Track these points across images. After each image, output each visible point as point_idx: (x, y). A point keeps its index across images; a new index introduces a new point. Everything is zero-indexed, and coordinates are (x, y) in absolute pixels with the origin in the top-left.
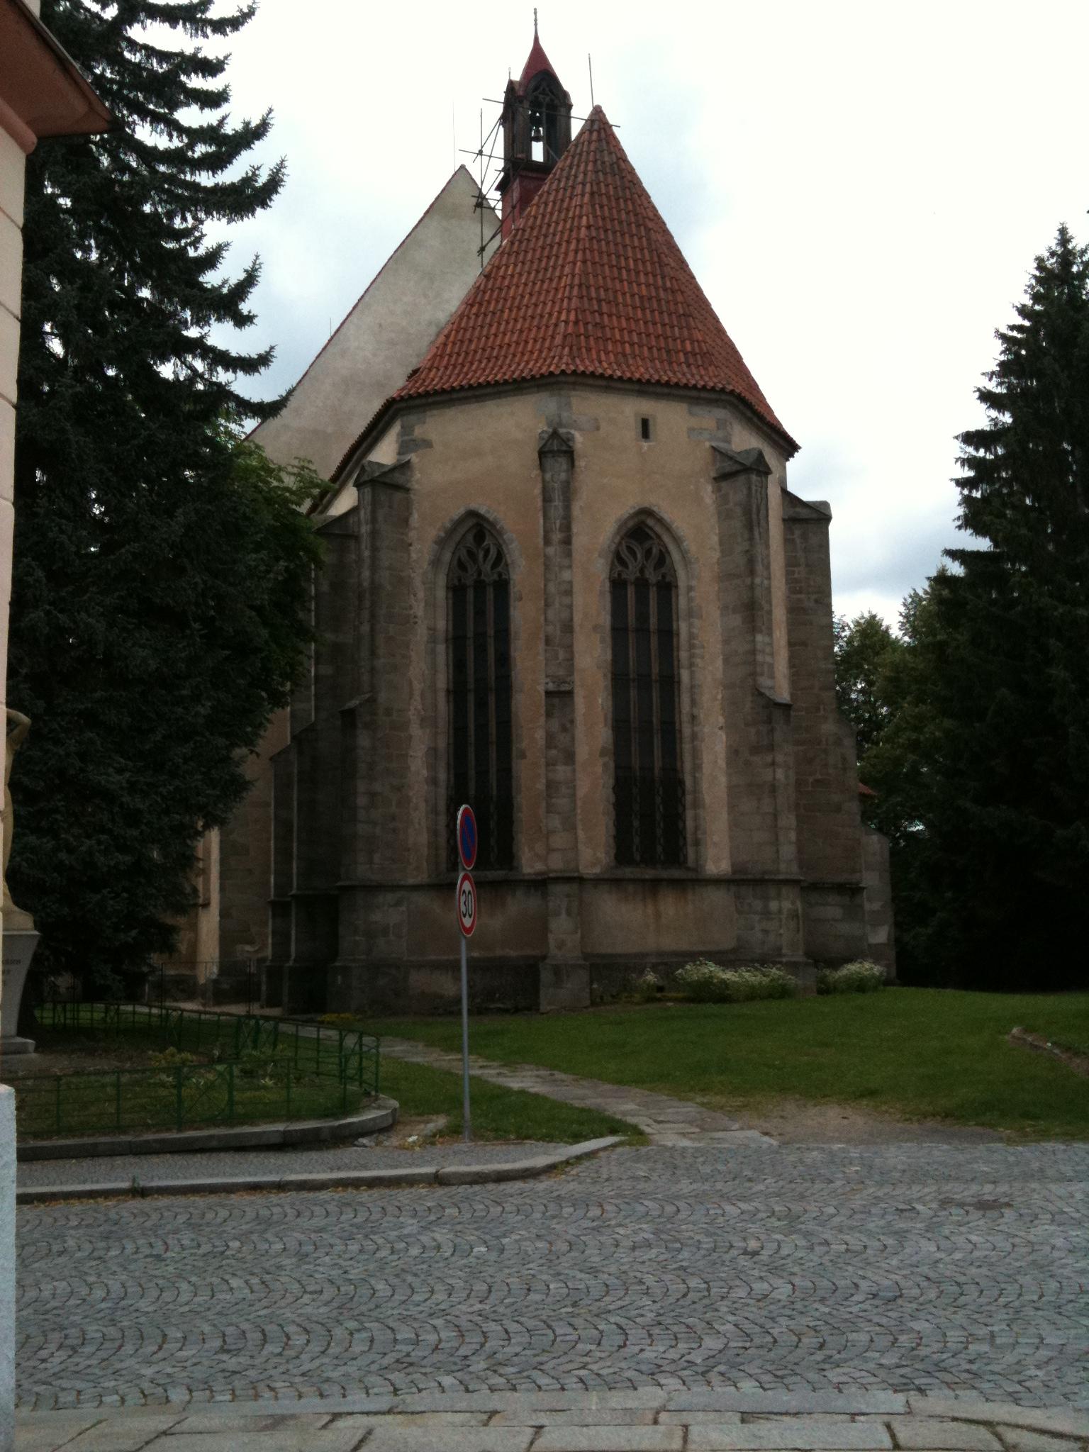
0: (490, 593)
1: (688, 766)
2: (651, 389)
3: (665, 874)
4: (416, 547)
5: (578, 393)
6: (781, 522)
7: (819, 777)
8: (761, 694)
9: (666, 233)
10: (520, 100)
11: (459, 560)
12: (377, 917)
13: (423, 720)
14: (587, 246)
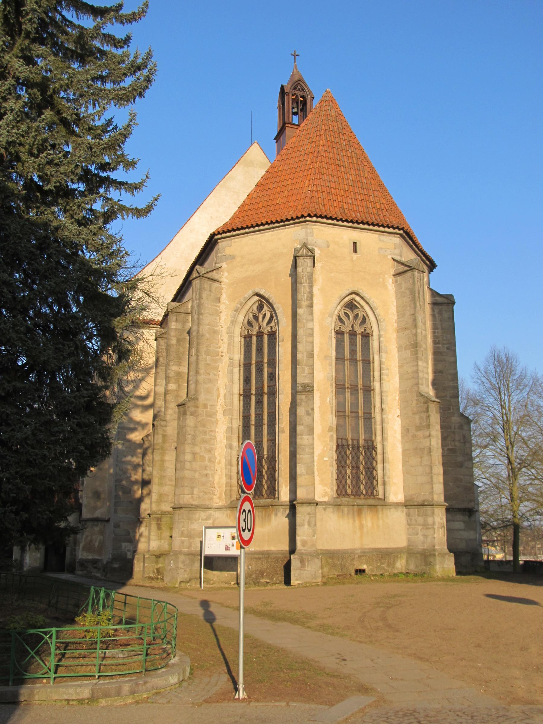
7: (450, 447)
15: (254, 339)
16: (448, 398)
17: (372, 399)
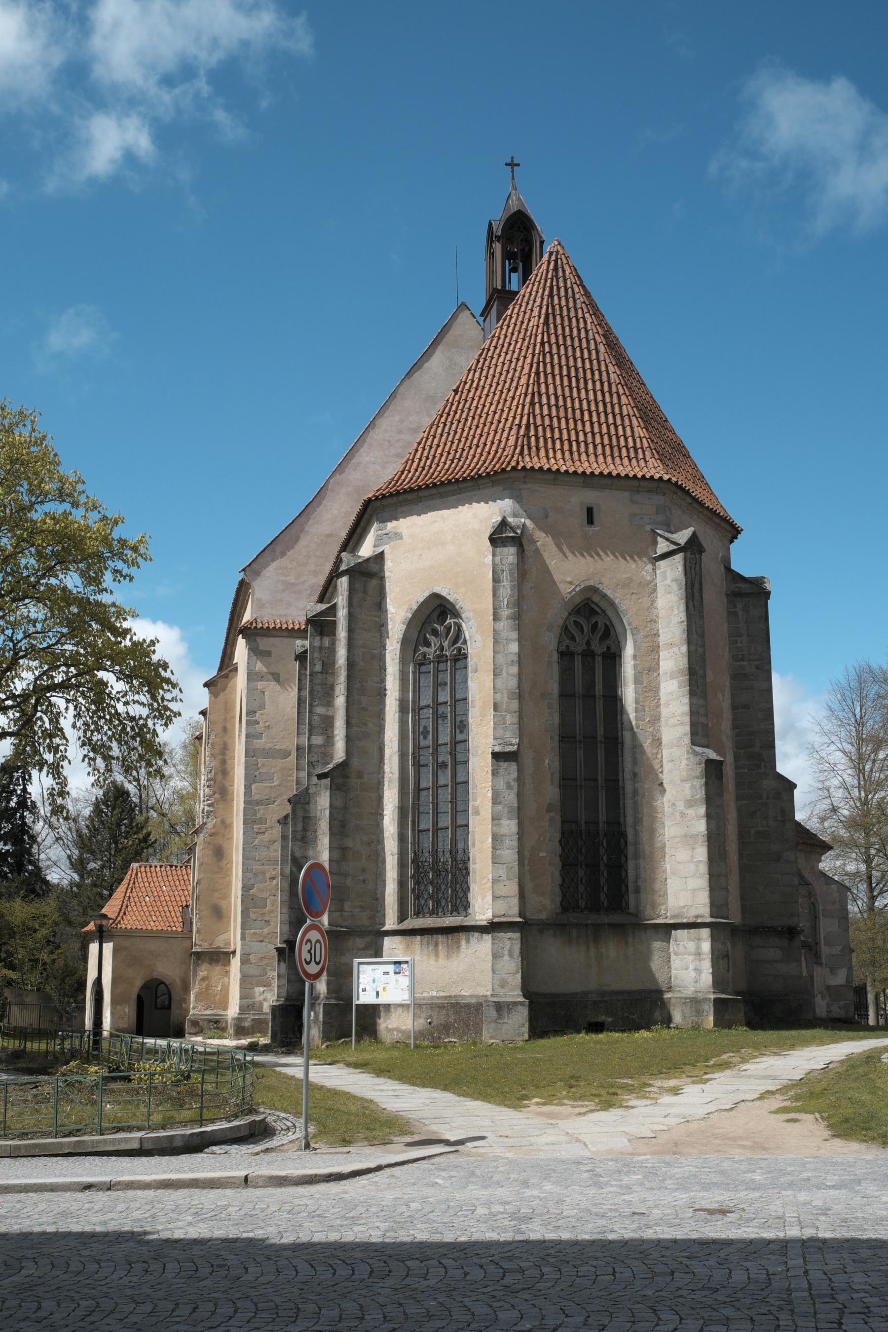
1: (630, 820)
3: (606, 919)
5: (529, 486)
6: (724, 597)
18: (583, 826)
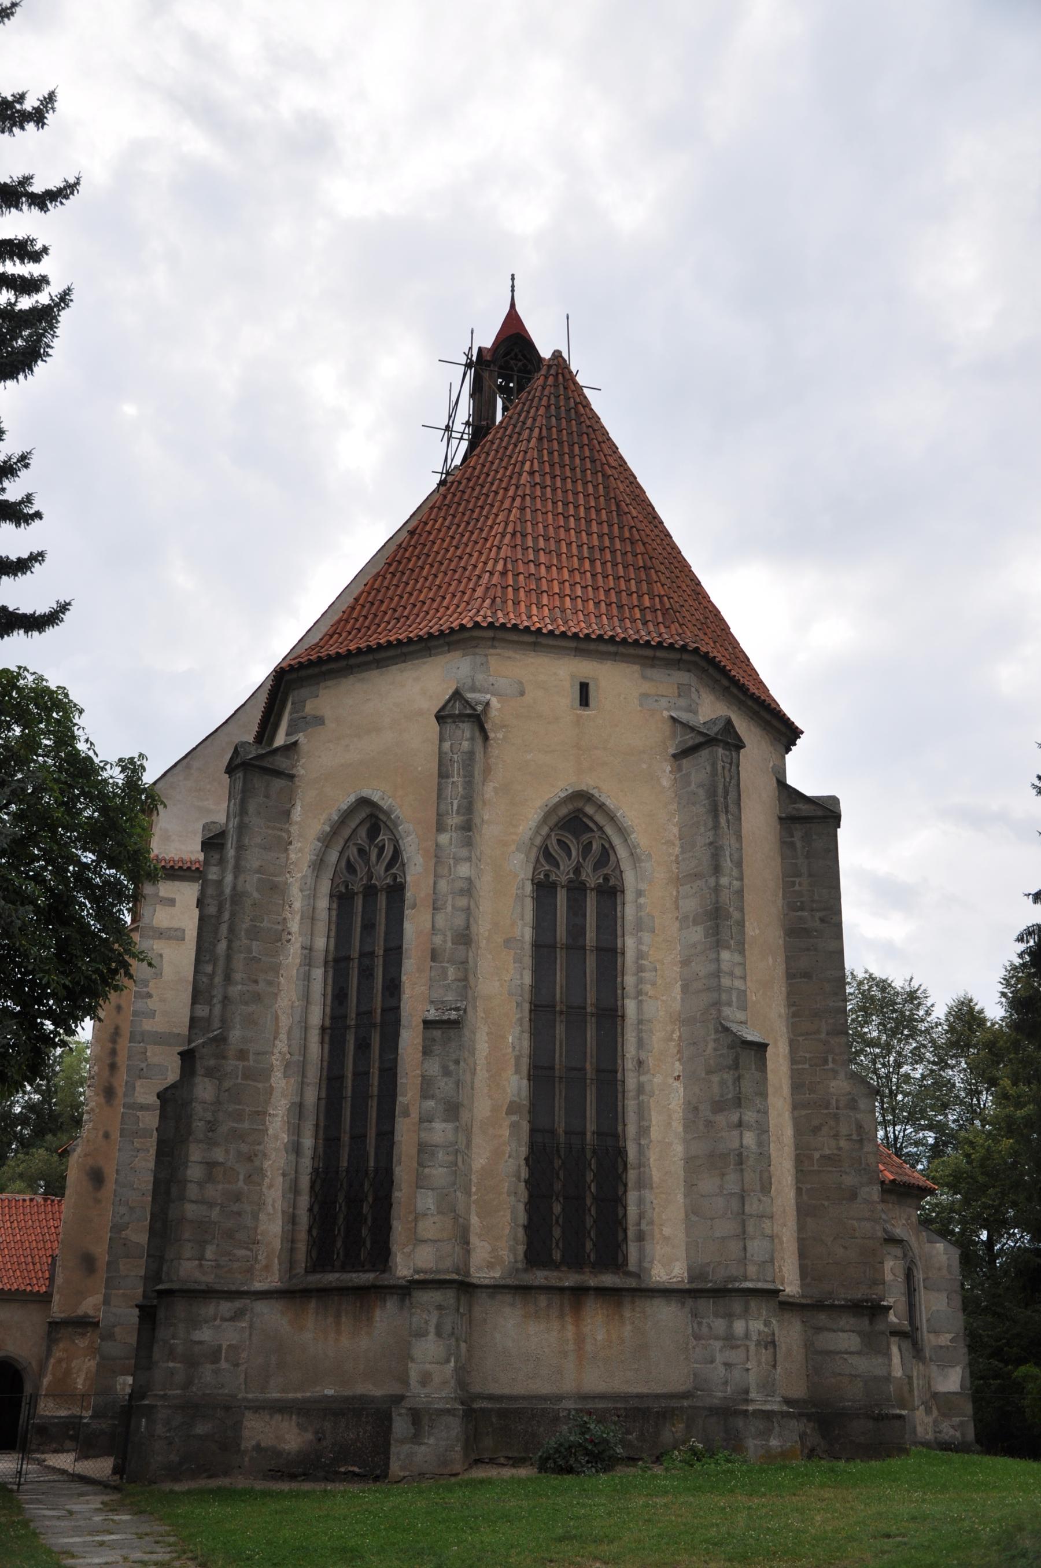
0: (382, 900)
1: (631, 1130)
2: (592, 646)
4: (297, 845)
5: (498, 651)
7: (827, 1152)
8: (727, 1030)
9: (631, 479)
10: (488, 364)
11: (348, 861)
12: (205, 1334)
13: (287, 1066)
14: (528, 492)
15: (359, 902)
16: (823, 1036)
17: (620, 1040)
18: (562, 1139)
